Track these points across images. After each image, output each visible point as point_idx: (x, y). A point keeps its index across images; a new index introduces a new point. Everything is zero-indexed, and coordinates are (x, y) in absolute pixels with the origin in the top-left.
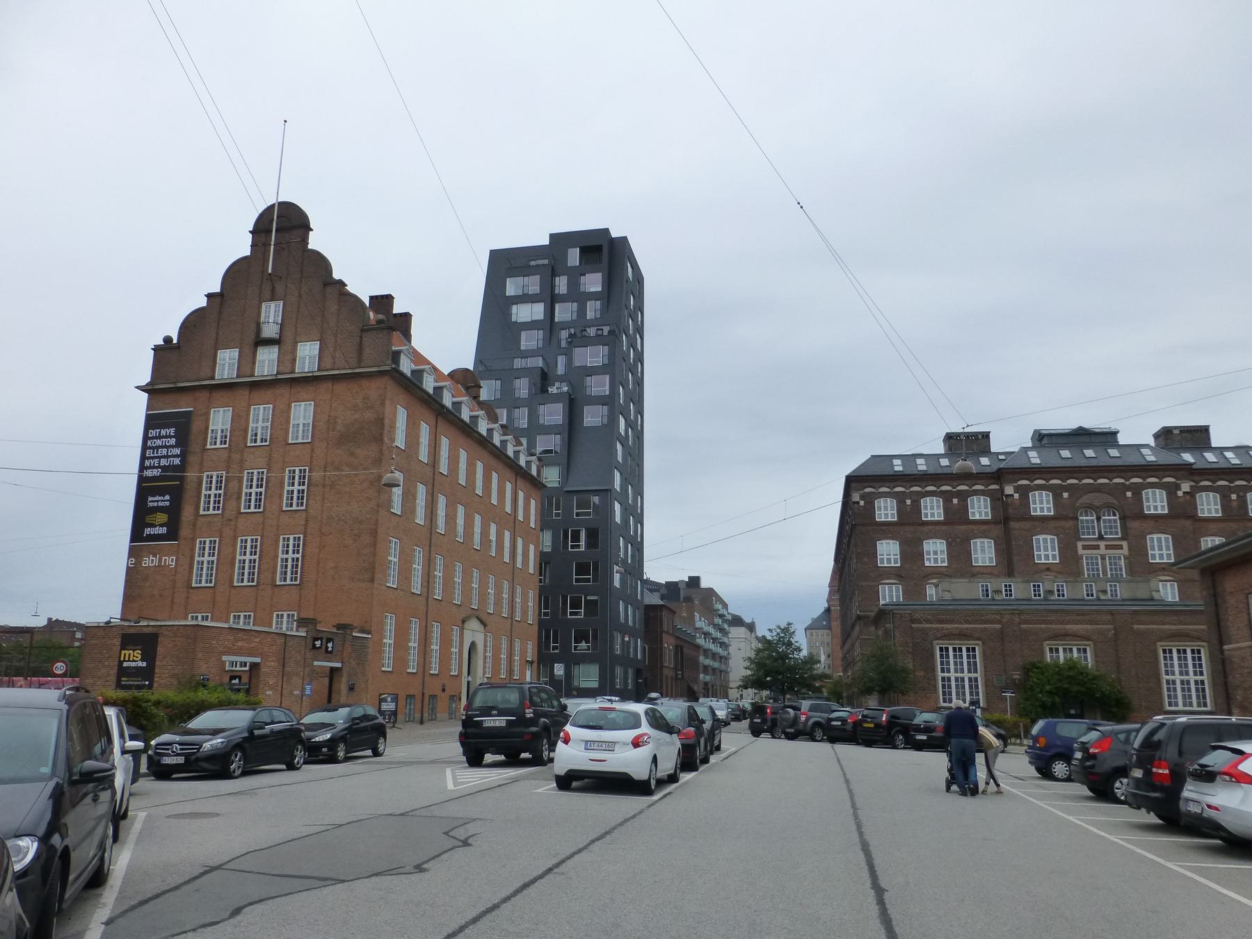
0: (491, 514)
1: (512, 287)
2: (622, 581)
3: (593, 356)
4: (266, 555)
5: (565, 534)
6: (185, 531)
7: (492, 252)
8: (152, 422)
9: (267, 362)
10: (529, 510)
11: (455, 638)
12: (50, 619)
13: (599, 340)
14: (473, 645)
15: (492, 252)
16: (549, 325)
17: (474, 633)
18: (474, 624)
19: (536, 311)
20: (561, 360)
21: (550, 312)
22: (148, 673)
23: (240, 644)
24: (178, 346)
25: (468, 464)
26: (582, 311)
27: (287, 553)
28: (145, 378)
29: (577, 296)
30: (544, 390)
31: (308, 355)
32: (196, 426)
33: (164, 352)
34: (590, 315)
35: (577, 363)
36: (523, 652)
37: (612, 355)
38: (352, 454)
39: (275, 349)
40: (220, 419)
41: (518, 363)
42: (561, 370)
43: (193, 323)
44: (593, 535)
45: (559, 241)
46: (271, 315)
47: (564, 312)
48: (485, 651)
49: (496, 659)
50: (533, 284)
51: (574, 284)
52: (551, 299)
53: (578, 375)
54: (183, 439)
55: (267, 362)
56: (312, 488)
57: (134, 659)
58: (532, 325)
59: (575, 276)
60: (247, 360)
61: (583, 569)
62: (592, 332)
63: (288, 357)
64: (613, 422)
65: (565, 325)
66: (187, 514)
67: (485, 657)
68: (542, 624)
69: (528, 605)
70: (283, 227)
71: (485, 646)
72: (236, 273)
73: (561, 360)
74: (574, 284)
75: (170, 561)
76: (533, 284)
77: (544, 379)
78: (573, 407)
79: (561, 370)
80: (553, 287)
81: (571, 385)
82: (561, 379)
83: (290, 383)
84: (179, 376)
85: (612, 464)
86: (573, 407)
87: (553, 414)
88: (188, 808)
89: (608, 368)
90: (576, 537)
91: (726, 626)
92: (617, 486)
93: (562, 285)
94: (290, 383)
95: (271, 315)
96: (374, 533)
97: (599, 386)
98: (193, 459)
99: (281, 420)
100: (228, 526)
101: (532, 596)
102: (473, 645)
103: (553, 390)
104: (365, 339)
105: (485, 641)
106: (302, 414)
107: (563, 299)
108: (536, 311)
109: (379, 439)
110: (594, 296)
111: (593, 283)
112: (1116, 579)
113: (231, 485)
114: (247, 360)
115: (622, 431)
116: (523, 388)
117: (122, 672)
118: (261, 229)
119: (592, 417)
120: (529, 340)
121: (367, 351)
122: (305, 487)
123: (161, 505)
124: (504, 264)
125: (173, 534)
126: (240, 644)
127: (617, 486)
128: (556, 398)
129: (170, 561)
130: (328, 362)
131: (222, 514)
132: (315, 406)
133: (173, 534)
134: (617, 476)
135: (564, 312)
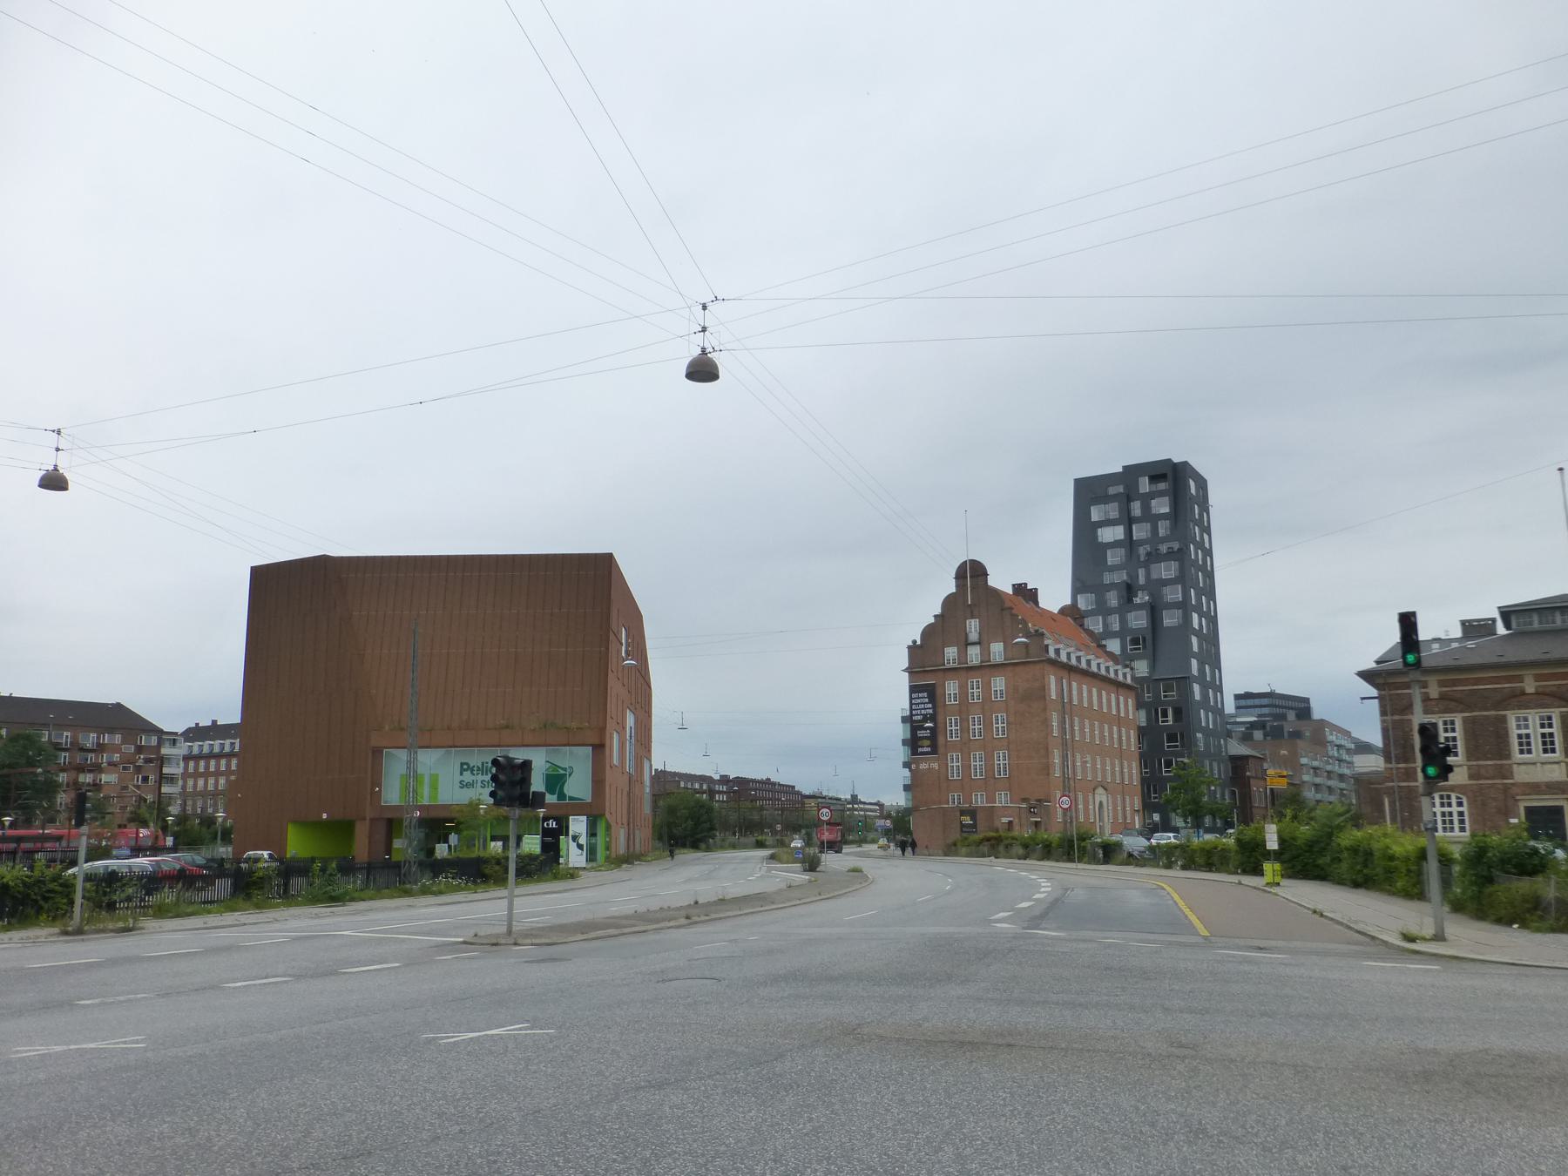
0: (1103, 718)
1: (1096, 514)
2: (1200, 646)
3: (1167, 570)
5: (1153, 709)
6: (941, 750)
7: (1076, 481)
8: (914, 689)
9: (974, 655)
10: (1126, 706)
12: (214, 722)
13: (1171, 555)
15: (1076, 481)
16: (1129, 543)
17: (1101, 796)
18: (1100, 790)
19: (1118, 533)
20: (1141, 572)
21: (1129, 532)
22: (974, 826)
24: (921, 646)
26: (1155, 530)
29: (1149, 517)
30: (1130, 600)
31: (997, 649)
32: (939, 691)
33: (913, 649)
34: (1162, 532)
35: (1154, 576)
36: (1132, 805)
37: (1182, 570)
40: (951, 688)
41: (1108, 578)
42: (1142, 580)
43: (928, 632)
44: (1178, 713)
45: (1132, 472)
46: (973, 627)
47: (1140, 532)
49: (1115, 809)
50: (1113, 510)
51: (1146, 508)
52: (1128, 521)
53: (1156, 586)
54: (932, 698)
57: (967, 820)
58: (1115, 544)
59: (1146, 499)
60: (963, 653)
61: (1172, 738)
62: (1164, 548)
63: (986, 652)
64: (1187, 620)
65: (1142, 542)
66: (941, 740)
68: (1144, 781)
69: (1132, 772)
70: (971, 573)
72: (949, 602)
73: (1141, 572)
74: (1146, 508)
75: (935, 766)
76: (1113, 510)
77: (1129, 590)
78: (1154, 611)
79: (1142, 580)
80: (1129, 511)
81: (1151, 595)
82: (1142, 588)
83: (988, 668)
84: (926, 663)
85: (1188, 653)
86: (1154, 611)
87: (1139, 620)
89: (1182, 579)
90: (1165, 714)
91: (1345, 757)
92: (1195, 671)
93: (1136, 509)
94: (988, 668)
95: (973, 627)
96: (1047, 749)
97: (1173, 594)
98: (940, 710)
100: (965, 746)
101: (1135, 765)
103: (1137, 600)
106: (999, 683)
107: (1139, 520)
108: (1118, 533)
109: (1044, 698)
110: (1163, 517)
111: (1162, 506)
112: (1127, 829)
114: (963, 653)
115: (1196, 625)
116: (1113, 599)
117: (963, 826)
118: (961, 575)
119: (1170, 619)
120: (1113, 557)
123: (922, 736)
124: (1088, 491)
125: (934, 751)
127: (1195, 671)
128: (1140, 607)
129: (935, 766)
133: (934, 751)
134: (1194, 662)
135: (1140, 532)
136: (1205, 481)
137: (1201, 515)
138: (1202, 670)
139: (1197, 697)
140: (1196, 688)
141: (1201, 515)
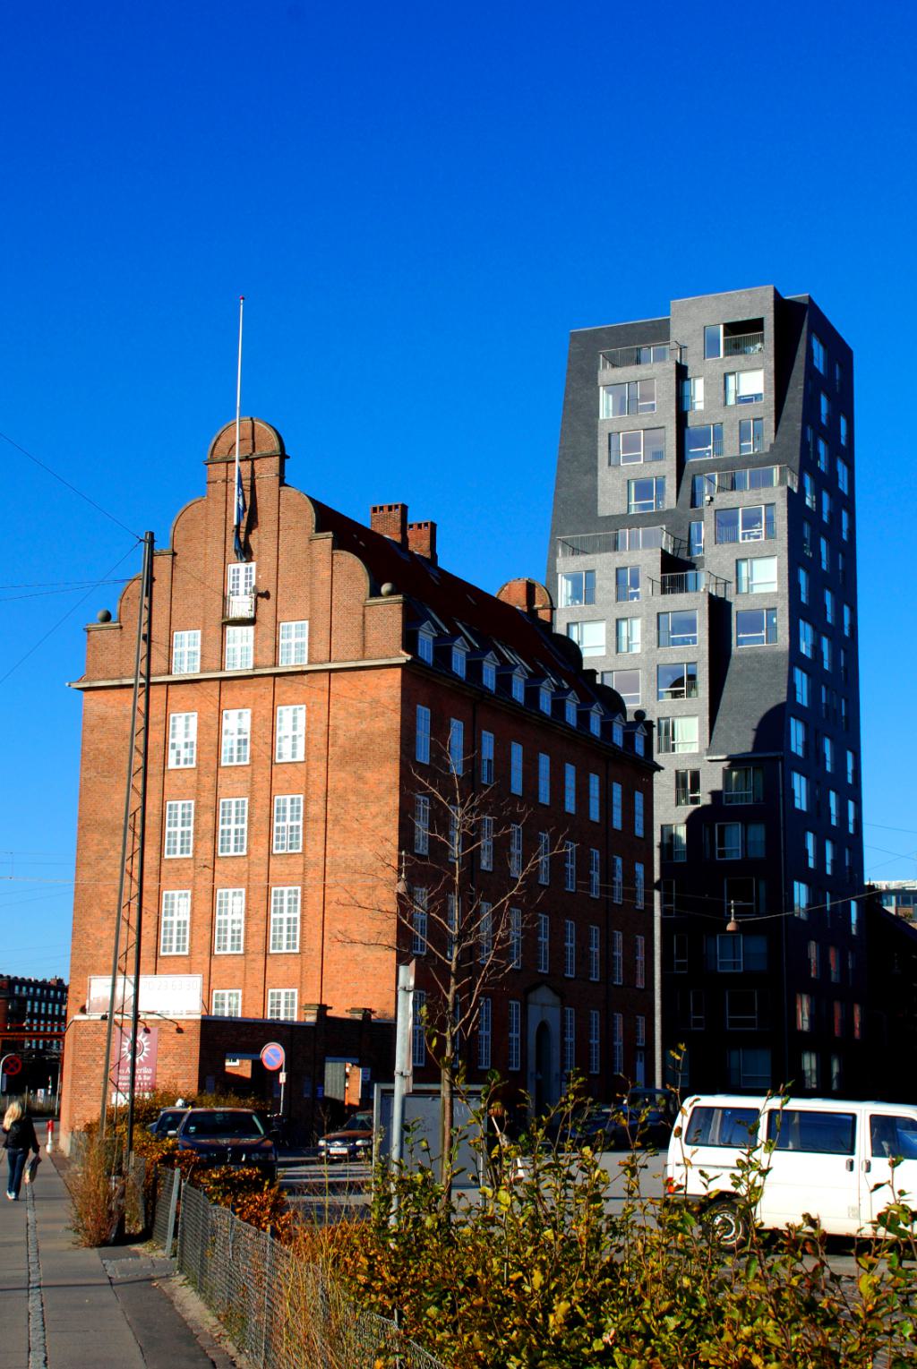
2: (814, 693)
4: (259, 914)
11: (515, 1018)
14: (543, 1028)
18: (544, 996)
23: (244, 1039)
25: (525, 762)
27: (286, 911)
28: (338, 1011)
38: (360, 778)
39: (250, 629)
48: (563, 1034)
55: (241, 649)
56: (310, 825)
60: (216, 649)
67: (563, 1044)
71: (563, 1027)
83: (271, 679)
88: (84, 1282)
94: (271, 679)
99: (266, 731)
102: (543, 1028)
104: (368, 618)
105: (563, 1020)
113: (203, 819)
114: (216, 649)
121: (372, 634)
122: (300, 823)
126: (244, 1039)
130: (322, 652)
131: (194, 858)
132: (309, 711)
136: (849, 353)
137: (835, 516)
138: (812, 744)
139: (801, 802)
140: (799, 784)
141: (835, 516)
